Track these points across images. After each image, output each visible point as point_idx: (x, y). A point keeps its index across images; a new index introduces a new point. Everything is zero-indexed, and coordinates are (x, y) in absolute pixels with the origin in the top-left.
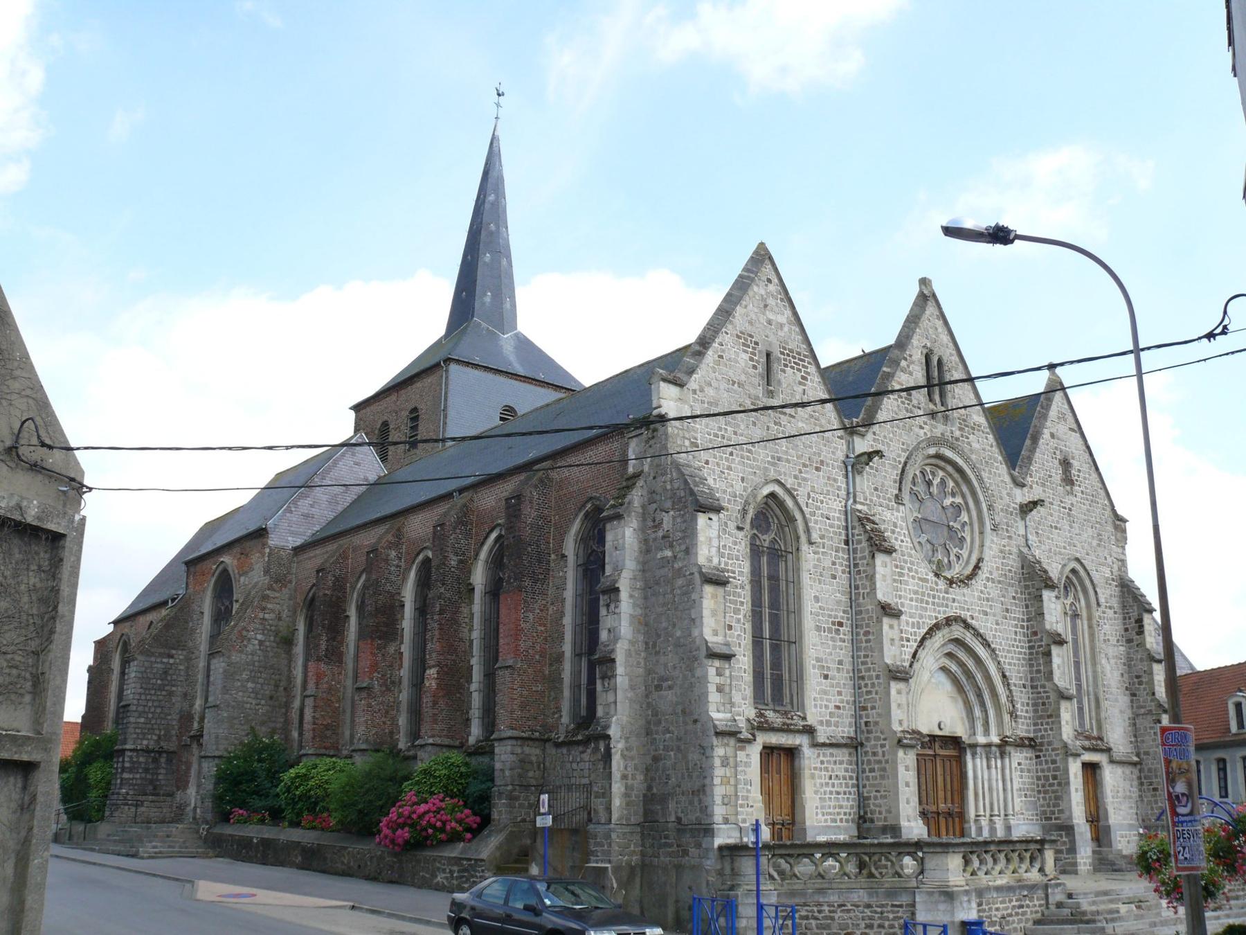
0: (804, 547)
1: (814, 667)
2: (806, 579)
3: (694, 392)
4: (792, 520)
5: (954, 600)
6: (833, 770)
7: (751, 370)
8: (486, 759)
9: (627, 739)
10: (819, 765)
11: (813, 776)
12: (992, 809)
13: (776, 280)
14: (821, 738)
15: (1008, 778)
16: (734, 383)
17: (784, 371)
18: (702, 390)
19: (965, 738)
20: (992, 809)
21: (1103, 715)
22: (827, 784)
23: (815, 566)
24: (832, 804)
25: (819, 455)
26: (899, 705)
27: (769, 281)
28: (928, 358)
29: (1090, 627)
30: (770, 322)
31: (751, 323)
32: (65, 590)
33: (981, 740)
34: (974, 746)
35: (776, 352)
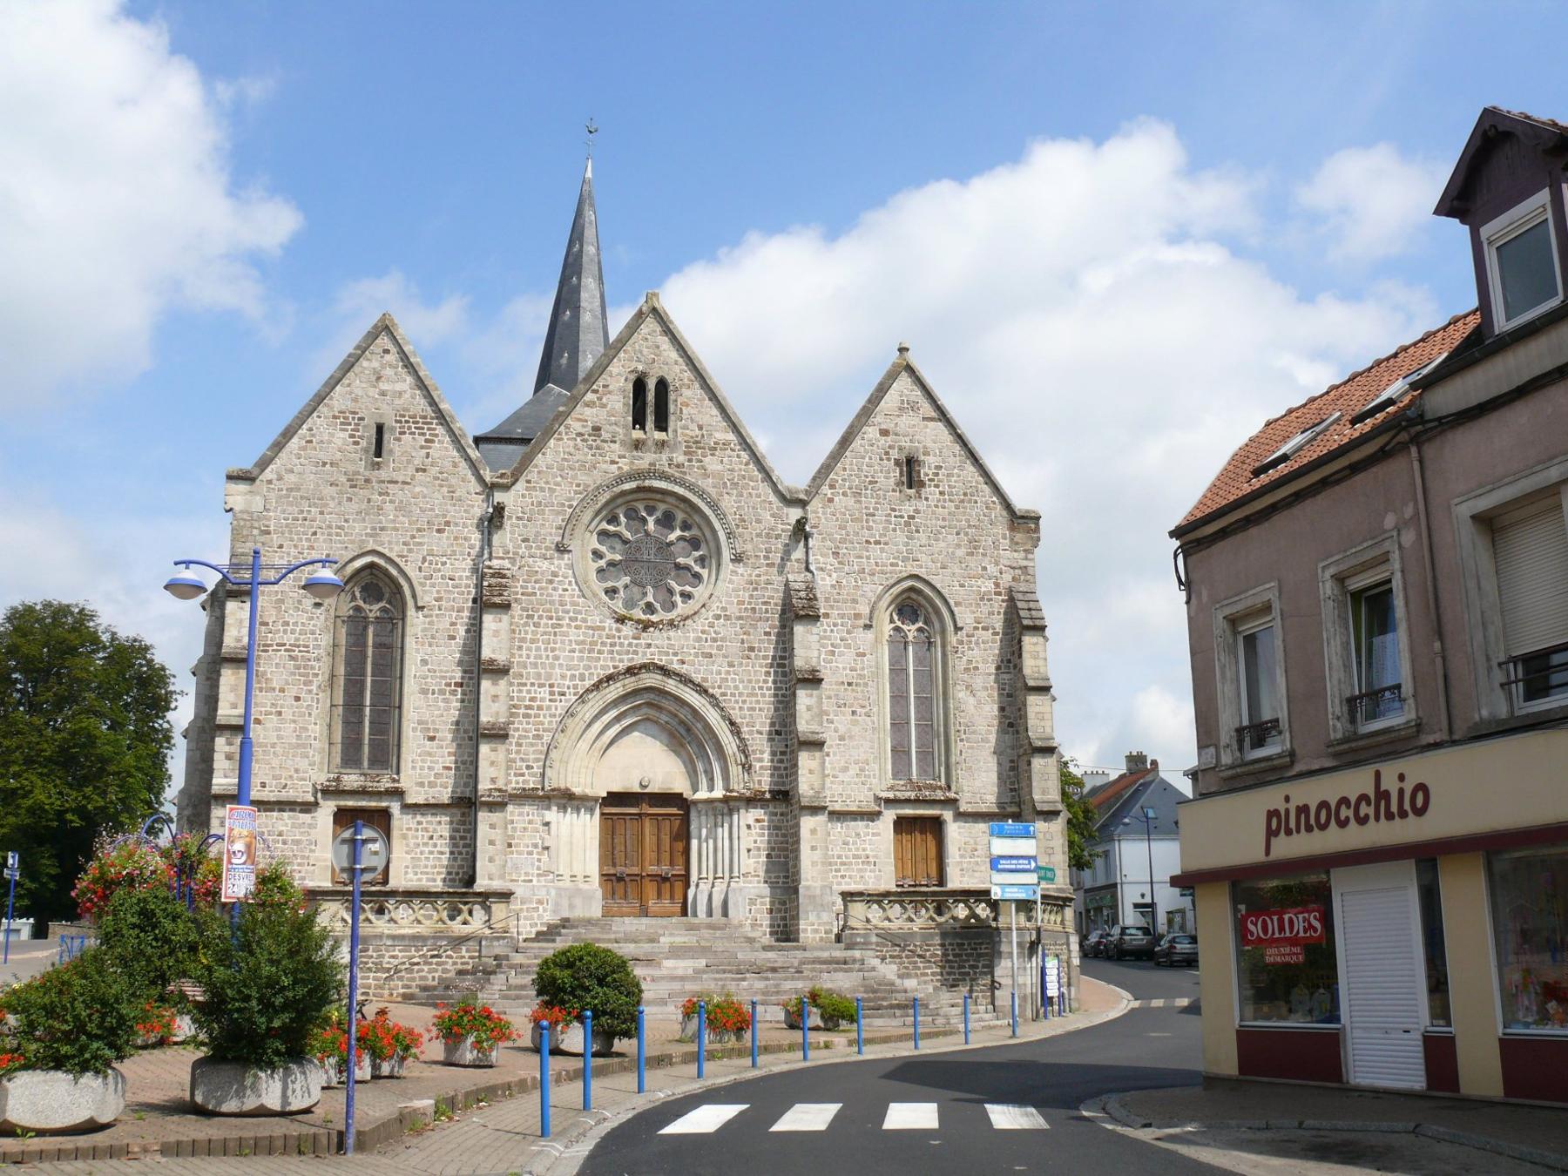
0: (411, 611)
1: (414, 730)
2: (410, 643)
3: (270, 482)
4: (399, 587)
5: (649, 645)
6: (435, 830)
7: (352, 448)
8: (1301, 922)
9: (195, 806)
10: (414, 826)
11: (404, 837)
12: (715, 872)
13: (393, 350)
14: (410, 801)
15: (735, 836)
16: (324, 464)
17: (399, 440)
18: (280, 478)
19: (688, 794)
20: (715, 872)
21: (953, 759)
22: (425, 844)
23: (424, 630)
24: (431, 863)
25: (444, 516)
26: (492, 763)
27: (387, 351)
28: (639, 386)
29: (944, 655)
30: (383, 394)
31: (355, 400)
32: (393, 740)
33: (702, 794)
34: (695, 803)
35: (389, 422)
